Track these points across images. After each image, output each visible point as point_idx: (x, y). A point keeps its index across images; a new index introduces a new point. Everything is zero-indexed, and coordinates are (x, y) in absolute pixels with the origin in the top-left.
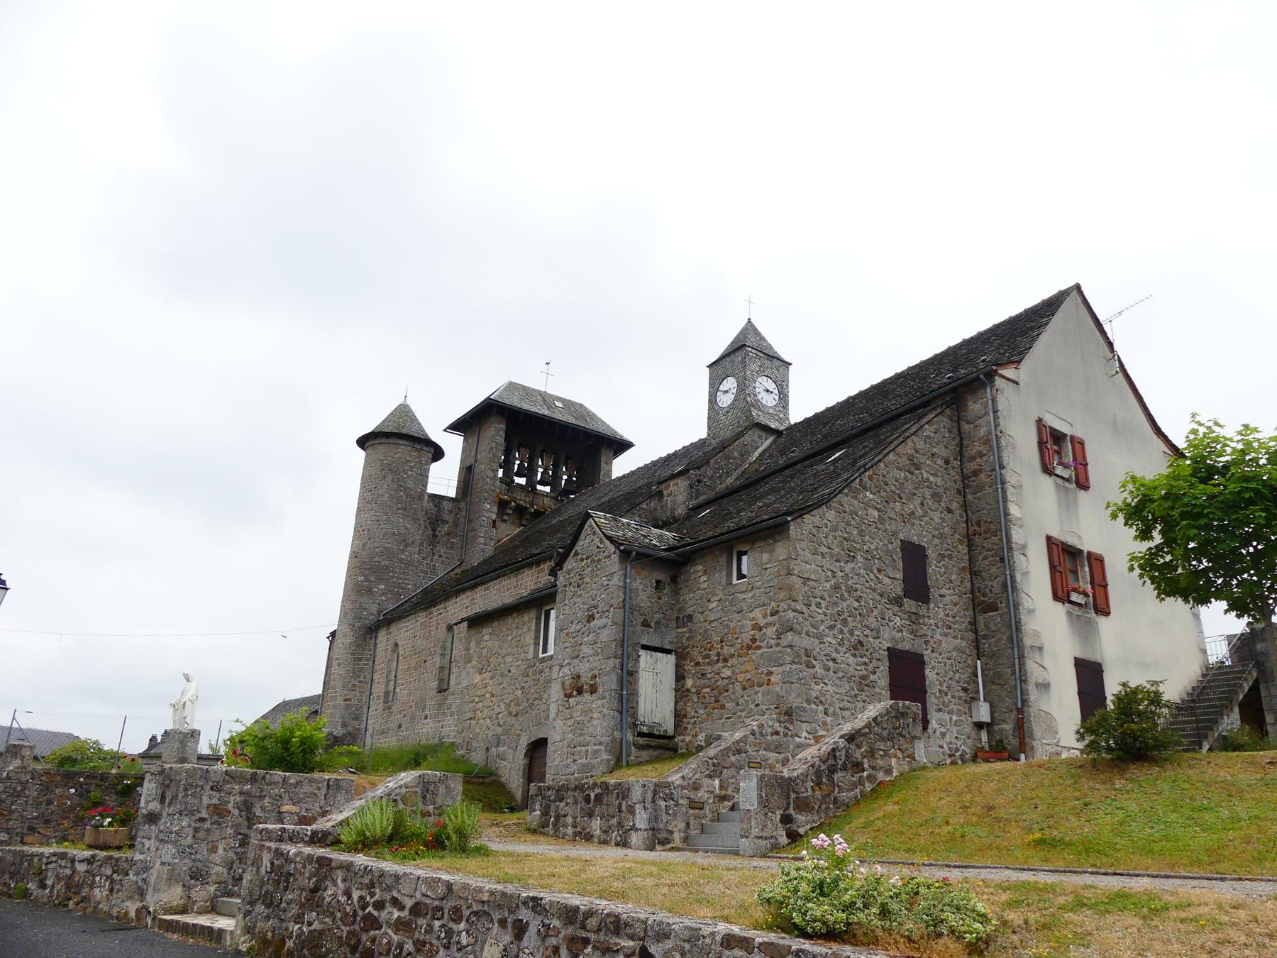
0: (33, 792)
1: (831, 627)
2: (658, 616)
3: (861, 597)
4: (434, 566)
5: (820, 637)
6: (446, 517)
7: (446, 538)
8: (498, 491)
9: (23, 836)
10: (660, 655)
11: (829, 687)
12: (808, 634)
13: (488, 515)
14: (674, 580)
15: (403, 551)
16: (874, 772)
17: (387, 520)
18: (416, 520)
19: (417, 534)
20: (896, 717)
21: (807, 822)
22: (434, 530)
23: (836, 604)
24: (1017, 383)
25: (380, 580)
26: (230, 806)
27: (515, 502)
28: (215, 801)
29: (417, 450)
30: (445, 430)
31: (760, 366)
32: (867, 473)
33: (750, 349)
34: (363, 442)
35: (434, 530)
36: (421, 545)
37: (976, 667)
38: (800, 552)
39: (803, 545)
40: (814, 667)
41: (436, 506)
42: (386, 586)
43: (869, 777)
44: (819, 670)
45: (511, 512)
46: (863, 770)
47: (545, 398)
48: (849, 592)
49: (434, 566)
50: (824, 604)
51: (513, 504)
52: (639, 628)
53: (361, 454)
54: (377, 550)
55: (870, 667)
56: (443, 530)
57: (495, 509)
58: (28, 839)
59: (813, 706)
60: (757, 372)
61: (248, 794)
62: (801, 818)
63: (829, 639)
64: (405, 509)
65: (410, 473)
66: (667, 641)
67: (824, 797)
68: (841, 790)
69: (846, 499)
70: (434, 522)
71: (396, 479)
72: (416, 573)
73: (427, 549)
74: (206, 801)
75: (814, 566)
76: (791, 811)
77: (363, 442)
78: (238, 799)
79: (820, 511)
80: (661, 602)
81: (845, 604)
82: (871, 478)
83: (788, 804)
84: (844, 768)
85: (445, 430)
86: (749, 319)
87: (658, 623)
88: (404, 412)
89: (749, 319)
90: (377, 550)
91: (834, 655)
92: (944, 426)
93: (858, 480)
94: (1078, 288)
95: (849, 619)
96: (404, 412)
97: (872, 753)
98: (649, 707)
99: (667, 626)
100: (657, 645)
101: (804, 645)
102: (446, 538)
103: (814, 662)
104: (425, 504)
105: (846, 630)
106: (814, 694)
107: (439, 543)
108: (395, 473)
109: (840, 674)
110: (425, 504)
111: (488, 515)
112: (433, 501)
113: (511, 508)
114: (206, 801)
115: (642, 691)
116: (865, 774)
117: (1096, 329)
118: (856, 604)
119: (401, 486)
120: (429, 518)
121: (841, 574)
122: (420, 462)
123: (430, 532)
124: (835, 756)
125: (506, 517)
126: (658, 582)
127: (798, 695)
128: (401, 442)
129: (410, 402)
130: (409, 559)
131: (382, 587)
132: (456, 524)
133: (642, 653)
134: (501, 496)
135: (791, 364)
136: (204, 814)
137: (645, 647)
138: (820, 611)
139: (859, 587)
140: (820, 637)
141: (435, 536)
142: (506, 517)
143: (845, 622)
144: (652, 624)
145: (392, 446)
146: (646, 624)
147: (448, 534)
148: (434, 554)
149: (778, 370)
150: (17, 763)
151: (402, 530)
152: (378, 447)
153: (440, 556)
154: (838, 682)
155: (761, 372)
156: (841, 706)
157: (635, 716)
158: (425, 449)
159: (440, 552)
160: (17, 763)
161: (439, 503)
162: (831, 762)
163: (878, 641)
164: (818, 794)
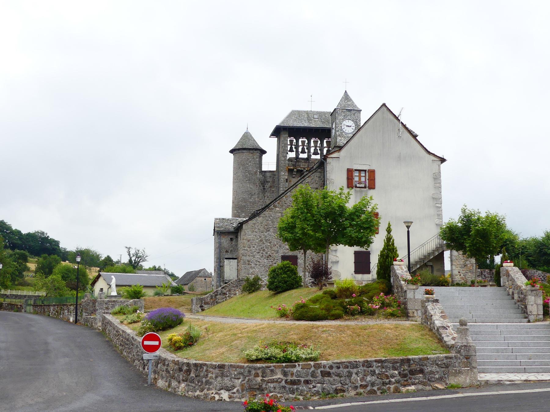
0: (91, 304)
1: (258, 253)
2: (231, 249)
3: (271, 242)
4: (266, 202)
5: (254, 256)
6: (268, 180)
7: (269, 189)
8: (287, 165)
9: (91, 314)
10: (231, 260)
11: (257, 270)
12: (249, 256)
13: (283, 177)
14: (237, 237)
15: (251, 198)
16: (230, 295)
17: (242, 186)
18: (254, 183)
19: (256, 189)
20: (239, 281)
21: (208, 307)
22: (264, 186)
23: (261, 246)
24: (339, 158)
25: (243, 212)
26: (110, 307)
27: (296, 169)
28: (106, 306)
29: (252, 153)
30: (270, 137)
31: (344, 116)
32: (277, 202)
33: (338, 110)
34: (232, 151)
35: (264, 186)
36: (258, 194)
37: (323, 256)
38: (247, 232)
39: (248, 230)
40: (251, 265)
41: (263, 176)
42: (245, 214)
43: (228, 296)
44: (253, 265)
45: (295, 173)
46: (227, 295)
47: (308, 114)
48: (266, 241)
49: (266, 202)
50: (256, 246)
51: (295, 170)
52: (224, 253)
53: (232, 155)
54: (240, 199)
55: (274, 262)
56: (267, 186)
57: (287, 174)
58: (92, 315)
59: (250, 275)
60: (343, 119)
61: (113, 304)
62: (205, 306)
63: (257, 256)
64: (249, 180)
65: (250, 164)
66: (234, 256)
67: (213, 301)
68: (218, 299)
69: (267, 212)
70: (263, 183)
71: (244, 168)
72: (258, 206)
73: (261, 195)
74: (104, 306)
75: (252, 236)
76: (203, 305)
77: (232, 151)
78: (111, 305)
79: (255, 219)
80: (232, 244)
81: (264, 245)
82: (279, 203)
83: (202, 303)
84: (220, 294)
85: (270, 137)
86: (346, 91)
87: (231, 251)
88: (247, 136)
89: (346, 91)
90: (240, 199)
91: (259, 260)
92: (317, 176)
93: (273, 205)
94: (384, 105)
95: (266, 249)
96: (247, 136)
97: (230, 291)
98: (228, 275)
99: (235, 251)
100: (231, 257)
101: (247, 259)
102: (269, 189)
103: (251, 263)
104: (258, 176)
105: (264, 253)
106: (250, 272)
107: (266, 192)
108: (243, 165)
109: (261, 266)
110: (258, 176)
111: (283, 177)
112: (262, 174)
113: (295, 172)
114: (104, 306)
115: (225, 270)
116: (227, 295)
117: (394, 119)
118: (269, 244)
119: (246, 170)
120: (261, 182)
121: (263, 236)
122: (254, 158)
123: (262, 188)
124: (217, 292)
125: (294, 176)
126: (231, 238)
127: (245, 273)
128: (244, 151)
129: (250, 131)
130: (254, 201)
131: (244, 214)
132: (274, 182)
133: (225, 260)
134: (289, 168)
135: (361, 110)
136: (104, 309)
137: (226, 259)
138: (254, 249)
139: (271, 239)
140: (254, 256)
141: (264, 189)
142: (294, 176)
143: (264, 250)
144: (229, 252)
145: (241, 154)
146: (227, 252)
147: (271, 187)
148: (265, 197)
149: (354, 115)
150: (87, 298)
151: (249, 189)
152: (236, 154)
153: (268, 197)
154: (260, 268)
155: (345, 118)
156: (261, 274)
157: (223, 278)
158: (255, 152)
159: (267, 195)
160: (87, 298)
161: (265, 174)
162: (216, 293)
163: (277, 254)
164: (212, 301)
